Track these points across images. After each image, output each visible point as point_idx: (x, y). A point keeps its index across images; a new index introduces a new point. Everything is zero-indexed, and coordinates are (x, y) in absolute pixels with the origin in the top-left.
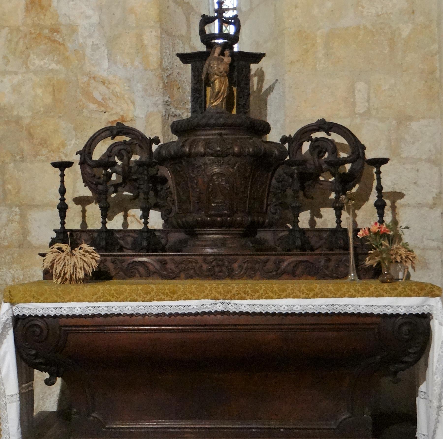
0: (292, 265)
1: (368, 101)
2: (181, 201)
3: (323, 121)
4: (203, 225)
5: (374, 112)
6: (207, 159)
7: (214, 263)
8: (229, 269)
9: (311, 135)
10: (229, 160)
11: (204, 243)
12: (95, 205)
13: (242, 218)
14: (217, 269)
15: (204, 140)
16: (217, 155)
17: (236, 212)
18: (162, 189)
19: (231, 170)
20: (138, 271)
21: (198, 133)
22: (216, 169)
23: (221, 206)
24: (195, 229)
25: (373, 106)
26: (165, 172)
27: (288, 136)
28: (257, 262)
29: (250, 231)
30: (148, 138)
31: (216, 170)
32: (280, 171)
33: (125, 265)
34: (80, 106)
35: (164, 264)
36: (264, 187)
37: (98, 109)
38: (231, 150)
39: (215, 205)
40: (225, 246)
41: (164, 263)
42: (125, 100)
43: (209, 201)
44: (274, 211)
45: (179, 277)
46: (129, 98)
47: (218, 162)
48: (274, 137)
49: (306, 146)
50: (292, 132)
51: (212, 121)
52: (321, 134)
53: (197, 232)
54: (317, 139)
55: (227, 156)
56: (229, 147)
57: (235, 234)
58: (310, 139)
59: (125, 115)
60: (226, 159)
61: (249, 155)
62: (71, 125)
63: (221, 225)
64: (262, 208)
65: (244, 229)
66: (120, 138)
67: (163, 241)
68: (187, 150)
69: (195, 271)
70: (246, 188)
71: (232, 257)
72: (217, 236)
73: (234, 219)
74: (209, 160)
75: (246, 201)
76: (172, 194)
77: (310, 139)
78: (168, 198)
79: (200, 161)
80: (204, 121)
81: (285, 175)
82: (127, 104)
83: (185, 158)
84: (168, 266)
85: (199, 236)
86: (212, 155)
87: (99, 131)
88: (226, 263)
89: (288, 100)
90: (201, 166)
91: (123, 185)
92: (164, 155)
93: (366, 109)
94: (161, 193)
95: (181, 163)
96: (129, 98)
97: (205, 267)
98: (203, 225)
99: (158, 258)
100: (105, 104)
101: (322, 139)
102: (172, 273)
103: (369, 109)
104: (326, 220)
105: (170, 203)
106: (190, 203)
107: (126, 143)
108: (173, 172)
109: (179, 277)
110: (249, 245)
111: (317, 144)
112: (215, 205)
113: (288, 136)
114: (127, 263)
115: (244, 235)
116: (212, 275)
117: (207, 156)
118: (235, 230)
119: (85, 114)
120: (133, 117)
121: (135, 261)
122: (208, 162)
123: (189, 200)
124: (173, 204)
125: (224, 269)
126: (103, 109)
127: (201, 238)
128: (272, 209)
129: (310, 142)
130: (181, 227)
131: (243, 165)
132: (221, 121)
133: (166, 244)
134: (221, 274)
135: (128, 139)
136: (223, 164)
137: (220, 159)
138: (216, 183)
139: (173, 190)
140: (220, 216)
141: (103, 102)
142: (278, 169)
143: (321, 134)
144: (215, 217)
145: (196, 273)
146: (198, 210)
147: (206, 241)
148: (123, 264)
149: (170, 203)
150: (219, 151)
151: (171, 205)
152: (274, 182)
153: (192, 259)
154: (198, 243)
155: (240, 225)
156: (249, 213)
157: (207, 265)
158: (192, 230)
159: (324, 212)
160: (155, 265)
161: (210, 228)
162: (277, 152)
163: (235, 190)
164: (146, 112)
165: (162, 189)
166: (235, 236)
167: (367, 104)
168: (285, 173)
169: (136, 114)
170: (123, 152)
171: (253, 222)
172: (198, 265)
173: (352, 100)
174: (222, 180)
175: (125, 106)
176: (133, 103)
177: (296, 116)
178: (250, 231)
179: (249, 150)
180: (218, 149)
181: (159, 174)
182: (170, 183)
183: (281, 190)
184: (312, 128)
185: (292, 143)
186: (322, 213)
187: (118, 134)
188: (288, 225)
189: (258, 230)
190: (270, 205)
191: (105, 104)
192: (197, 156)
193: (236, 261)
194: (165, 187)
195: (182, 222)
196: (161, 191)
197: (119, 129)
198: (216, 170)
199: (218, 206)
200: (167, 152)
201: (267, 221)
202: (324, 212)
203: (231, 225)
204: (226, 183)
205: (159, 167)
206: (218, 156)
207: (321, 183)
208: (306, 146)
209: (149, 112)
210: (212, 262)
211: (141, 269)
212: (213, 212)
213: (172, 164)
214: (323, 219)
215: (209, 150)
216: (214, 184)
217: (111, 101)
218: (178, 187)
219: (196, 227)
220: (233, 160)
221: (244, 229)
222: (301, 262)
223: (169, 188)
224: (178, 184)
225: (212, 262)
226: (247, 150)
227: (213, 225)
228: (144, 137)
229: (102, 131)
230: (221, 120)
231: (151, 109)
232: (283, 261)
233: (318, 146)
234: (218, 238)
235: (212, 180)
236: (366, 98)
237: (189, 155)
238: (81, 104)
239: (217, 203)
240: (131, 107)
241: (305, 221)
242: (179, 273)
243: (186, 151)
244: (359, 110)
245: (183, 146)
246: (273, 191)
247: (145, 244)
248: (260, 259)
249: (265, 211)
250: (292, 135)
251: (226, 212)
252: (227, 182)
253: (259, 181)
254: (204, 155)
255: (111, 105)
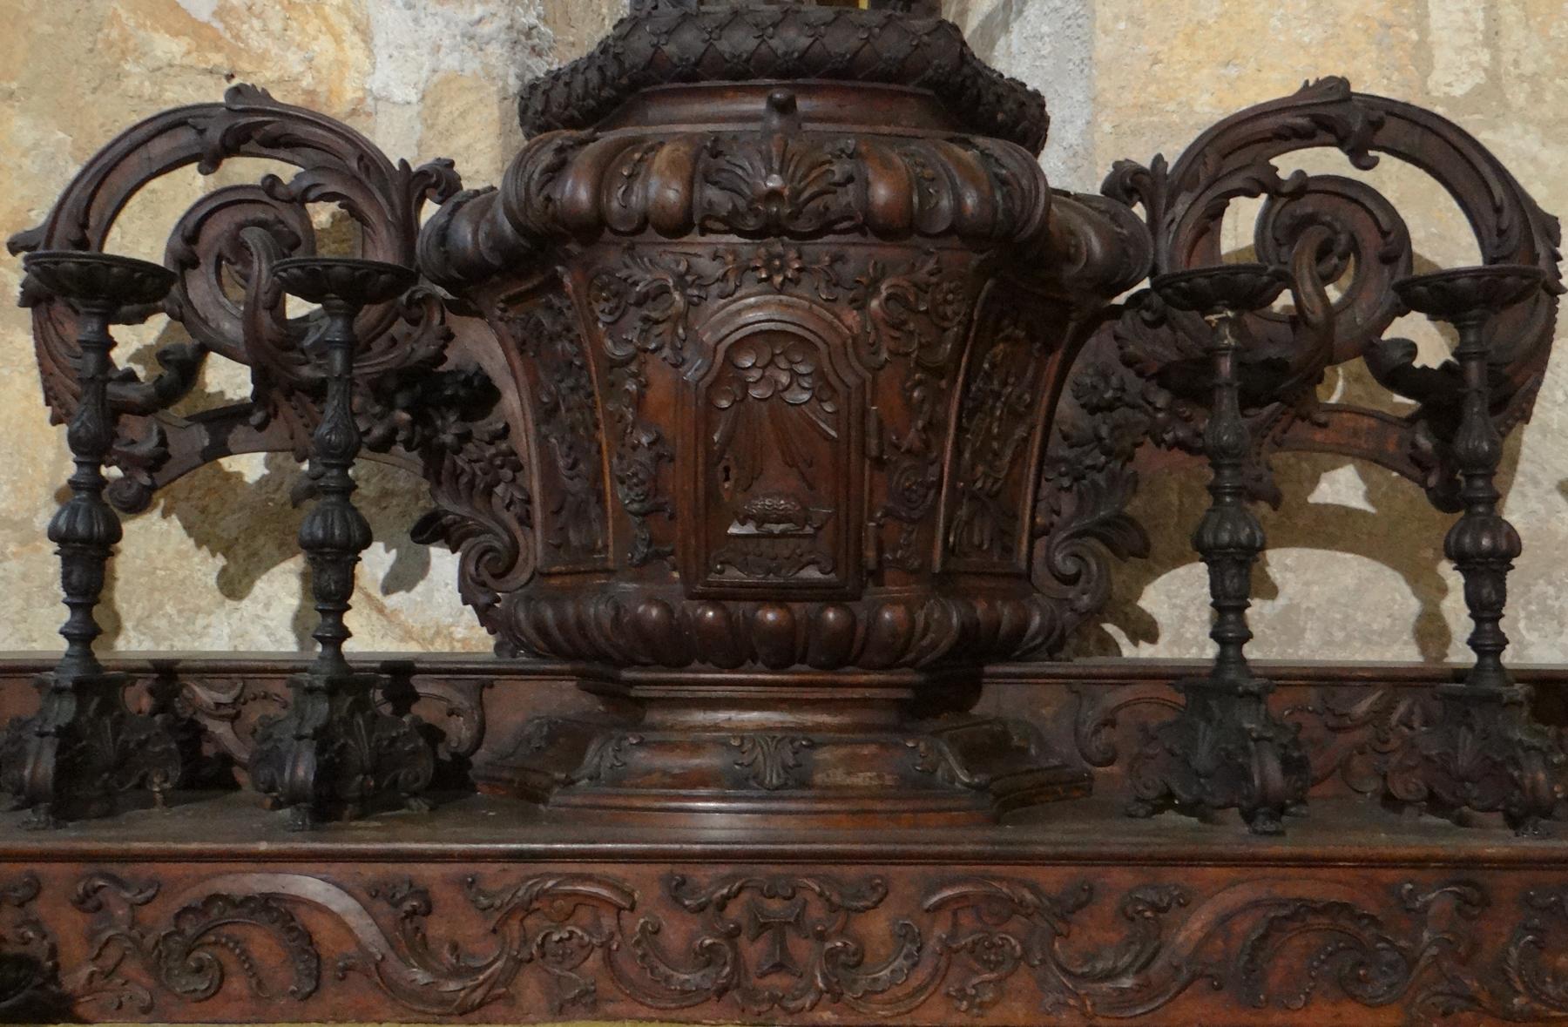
0: (1243, 925)
1: (1492, 37)
2: (558, 504)
3: (1337, 89)
4: (675, 647)
5: (1518, 96)
6: (704, 252)
7: (734, 911)
8: (832, 955)
9: (1274, 162)
10: (837, 259)
11: (676, 762)
12: (165, 525)
13: (910, 612)
14: (754, 951)
15: (689, 138)
16: (769, 224)
17: (877, 576)
18: (465, 437)
19: (852, 318)
20: (245, 957)
21: (654, 112)
22: (751, 307)
23: (783, 534)
24: (627, 674)
25: (1516, 63)
26: (480, 345)
27: (1147, 164)
28: (1016, 907)
29: (945, 684)
30: (395, 163)
31: (757, 310)
32: (1100, 347)
33: (159, 917)
34: (110, 45)
35: (413, 913)
36: (1021, 432)
37: (191, 60)
38: (848, 196)
39: (750, 529)
40: (804, 784)
41: (409, 914)
42: (325, 19)
43: (713, 510)
44: (1070, 567)
45: (509, 999)
46: (343, 10)
47: (768, 265)
48: (1072, 162)
49: (1241, 225)
50: (1166, 141)
51: (740, 42)
52: (1325, 161)
53: (637, 692)
54: (1303, 185)
55: (826, 228)
56: (839, 170)
57: (865, 703)
58: (1266, 183)
59: (322, 89)
60: (820, 250)
61: (959, 229)
62: (61, 135)
63: (784, 651)
64: (1008, 550)
65: (918, 678)
66: (246, 170)
67: (460, 730)
68: (584, 195)
69: (609, 960)
70: (934, 427)
71: (852, 872)
72: (754, 716)
73: (862, 615)
74: (715, 257)
75: (934, 508)
76: (518, 468)
77: (1266, 183)
78: (499, 490)
79: (658, 264)
80: (690, 41)
81: (1130, 375)
82: (338, 39)
83: (574, 248)
84: (436, 928)
85: (655, 716)
86: (731, 224)
87: (136, 128)
88: (816, 911)
89: (1106, 32)
90: (664, 290)
91: (257, 417)
92: (470, 246)
93: (1479, 78)
94: (461, 461)
95: (555, 284)
96: (343, 10)
97: (677, 933)
98: (675, 647)
99: (370, 871)
100: (228, 36)
101: (1334, 187)
102: (456, 973)
103: (1494, 77)
104: (1291, 608)
105: (509, 517)
106: (603, 518)
107: (279, 190)
108: (529, 346)
109: (509, 999)
110: (953, 778)
111: (1307, 205)
112: (750, 529)
113: (1147, 164)
114: (175, 906)
115: (915, 710)
116: (722, 992)
117: (704, 231)
118: (862, 680)
119: (131, 84)
120: (361, 100)
121: (227, 899)
122: (706, 265)
123: (601, 498)
124: (526, 520)
125: (802, 949)
126: (216, 59)
127: (662, 727)
128: (1059, 558)
129: (1264, 197)
130: (556, 652)
131: (922, 288)
132: (793, 39)
133: (478, 743)
134: (778, 981)
135: (287, 172)
136: (796, 282)
137: (779, 248)
138: (754, 393)
139: (524, 442)
140: (779, 596)
141: (216, 24)
142: (1092, 341)
143: (1325, 161)
144: (749, 605)
145: (617, 975)
146: (645, 561)
147: (696, 747)
148: (147, 912)
149: (509, 517)
150: (774, 195)
151: (515, 526)
152: (1067, 405)
153: (600, 882)
154: (642, 758)
155: (895, 653)
156: (945, 583)
157: (695, 923)
158: (621, 674)
159: (1287, 568)
160: (351, 920)
161: (721, 668)
162: (1096, 245)
163: (873, 443)
164: (425, 73)
165: (465, 437)
166: (868, 717)
167: (1485, 57)
168: (1128, 362)
169: (375, 84)
170: (252, 236)
171: (969, 632)
172: (635, 923)
173: (1414, 36)
174: (794, 375)
175: (323, 47)
176: (364, 32)
177: (1144, 108)
178: (945, 684)
179: (958, 200)
180: (774, 182)
181: (453, 356)
182: (512, 401)
183: (1108, 452)
184: (1269, 123)
185: (1171, 204)
186: (1274, 572)
187: (236, 143)
188: (1110, 628)
189: (989, 669)
190: (1045, 531)
191: (228, 36)
192: (639, 230)
193: (882, 893)
194: (482, 428)
195: (562, 625)
196: (458, 451)
197: (250, 123)
198: (760, 315)
199: (771, 535)
200: (484, 227)
201: (1036, 620)
202: (1287, 568)
203: (843, 652)
204: (817, 398)
205: (455, 322)
206: (767, 230)
207: (1323, 418)
208: (1241, 225)
209: (440, 75)
210: (722, 905)
211: (263, 943)
212: (734, 575)
213: (511, 301)
214: (1281, 601)
215: (712, 193)
216: (741, 400)
217: (257, 24)
218: (544, 429)
219: (631, 663)
220: (860, 255)
221: (918, 678)
222: (1305, 909)
223: (506, 432)
224: (546, 414)
225: (722, 905)
226: (946, 203)
227: (734, 648)
228: (370, 160)
229: (150, 127)
230: (791, 34)
231: (450, 62)
232: (1185, 902)
233: (1311, 220)
234: (765, 730)
235: (727, 373)
236: (1481, 26)
237: (592, 228)
238: (115, 34)
239: (761, 520)
240: (355, 53)
241: (1191, 613)
242: (509, 976)
243: (574, 200)
244: (1449, 85)
245: (556, 171)
246: (1063, 460)
247: (303, 769)
248: (1034, 888)
249: (1023, 565)
250: (1171, 160)
251: (812, 573)
252: (824, 386)
253: (998, 395)
254: (679, 226)
255: (257, 42)
